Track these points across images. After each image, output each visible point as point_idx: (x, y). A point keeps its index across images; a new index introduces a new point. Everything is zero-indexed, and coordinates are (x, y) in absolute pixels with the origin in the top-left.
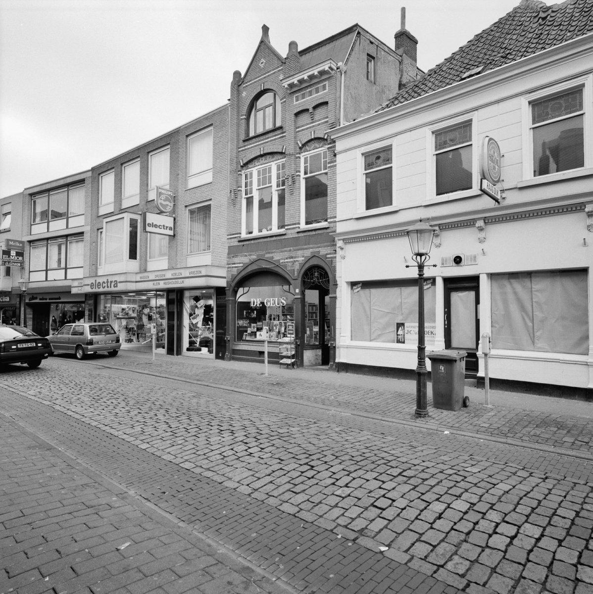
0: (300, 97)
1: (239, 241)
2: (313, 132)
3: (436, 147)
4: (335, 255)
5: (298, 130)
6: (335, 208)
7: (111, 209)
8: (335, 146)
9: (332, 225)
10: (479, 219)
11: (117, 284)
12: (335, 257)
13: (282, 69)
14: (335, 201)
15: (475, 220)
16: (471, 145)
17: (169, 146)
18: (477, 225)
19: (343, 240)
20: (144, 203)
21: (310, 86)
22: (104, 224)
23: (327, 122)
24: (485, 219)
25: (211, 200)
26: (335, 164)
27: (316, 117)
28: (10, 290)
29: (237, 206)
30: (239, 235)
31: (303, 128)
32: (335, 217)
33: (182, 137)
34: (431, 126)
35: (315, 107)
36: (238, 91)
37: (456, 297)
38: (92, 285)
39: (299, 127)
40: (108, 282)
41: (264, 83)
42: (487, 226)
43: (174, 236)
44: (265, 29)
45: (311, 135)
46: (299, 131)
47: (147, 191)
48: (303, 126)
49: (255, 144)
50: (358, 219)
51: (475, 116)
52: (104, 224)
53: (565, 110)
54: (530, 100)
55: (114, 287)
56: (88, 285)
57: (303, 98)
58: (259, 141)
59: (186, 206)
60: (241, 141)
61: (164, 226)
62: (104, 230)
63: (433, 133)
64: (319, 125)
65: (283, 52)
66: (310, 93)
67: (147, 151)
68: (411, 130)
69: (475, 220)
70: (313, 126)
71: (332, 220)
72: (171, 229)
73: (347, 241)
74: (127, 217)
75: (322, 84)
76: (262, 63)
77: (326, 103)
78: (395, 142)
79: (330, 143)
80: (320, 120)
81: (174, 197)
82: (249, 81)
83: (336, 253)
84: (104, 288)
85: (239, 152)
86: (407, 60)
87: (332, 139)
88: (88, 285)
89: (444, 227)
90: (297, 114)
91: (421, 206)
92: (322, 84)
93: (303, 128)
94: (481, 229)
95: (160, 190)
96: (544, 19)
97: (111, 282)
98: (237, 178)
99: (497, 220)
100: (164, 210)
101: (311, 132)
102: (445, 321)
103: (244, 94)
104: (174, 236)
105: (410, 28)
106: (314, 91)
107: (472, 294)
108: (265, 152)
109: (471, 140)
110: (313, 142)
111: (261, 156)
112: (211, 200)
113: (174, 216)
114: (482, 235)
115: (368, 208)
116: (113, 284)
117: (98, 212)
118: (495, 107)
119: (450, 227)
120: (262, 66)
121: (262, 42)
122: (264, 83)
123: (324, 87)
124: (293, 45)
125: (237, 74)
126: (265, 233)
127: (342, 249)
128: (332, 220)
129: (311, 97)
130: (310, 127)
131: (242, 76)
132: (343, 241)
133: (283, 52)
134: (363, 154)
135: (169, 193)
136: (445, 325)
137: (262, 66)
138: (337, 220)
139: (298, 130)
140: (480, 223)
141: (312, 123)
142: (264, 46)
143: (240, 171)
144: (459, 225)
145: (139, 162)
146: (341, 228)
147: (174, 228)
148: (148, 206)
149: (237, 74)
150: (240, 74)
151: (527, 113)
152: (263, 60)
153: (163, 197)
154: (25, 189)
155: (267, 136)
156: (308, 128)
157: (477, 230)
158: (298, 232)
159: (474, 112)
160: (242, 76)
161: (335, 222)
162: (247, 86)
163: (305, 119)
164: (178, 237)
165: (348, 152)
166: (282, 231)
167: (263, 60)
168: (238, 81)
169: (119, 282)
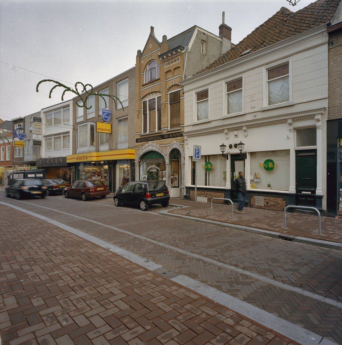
0: (170, 63)
1: (141, 136)
2: (174, 82)
3: (227, 90)
4: (184, 143)
5: (167, 80)
6: (183, 120)
7: (82, 119)
8: (183, 89)
9: (182, 128)
10: (289, 119)
11: (87, 157)
12: (184, 144)
13: (159, 50)
14: (183, 116)
15: (242, 127)
16: (289, 76)
17: (108, 88)
18: (316, 118)
19: (187, 136)
20: (97, 116)
21: (172, 58)
22: (79, 127)
23: (180, 77)
24: (247, 126)
25: (128, 115)
26: (184, 97)
27: (175, 74)
28: (36, 161)
29: (140, 119)
30: (141, 133)
31: (169, 79)
32: (184, 124)
33: (114, 84)
34: (225, 80)
35: (175, 69)
36: (140, 60)
37: (237, 163)
38: (77, 158)
39: (167, 79)
40: (83, 157)
41: (151, 57)
42: (229, 132)
43: (111, 133)
44: (152, 28)
45: (173, 83)
46: (167, 81)
47: (99, 111)
48: (169, 78)
49: (148, 87)
50: (193, 125)
51: (291, 60)
52: (79, 127)
53: (205, 97)
54: (267, 68)
55: (86, 159)
56: (75, 158)
57: (169, 65)
58: (150, 86)
59: (117, 118)
60: (141, 86)
61: (106, 129)
62: (79, 130)
63: (226, 83)
64: (176, 78)
65: (160, 40)
66: (172, 62)
67: (98, 90)
68: (309, 49)
69: (314, 115)
70: (174, 79)
71: (182, 126)
72: (109, 130)
73: (189, 136)
74: (89, 124)
75: (178, 58)
76: (151, 46)
77: (179, 67)
78: (210, 88)
79: (182, 87)
80: (177, 76)
81: (111, 114)
82: (145, 55)
83: (184, 142)
84: (82, 159)
85: (140, 91)
86: (225, 40)
87: (182, 85)
88: (75, 158)
89: (299, 119)
90: (166, 73)
91: (260, 111)
92: (178, 58)
93: (169, 79)
94: (245, 131)
95: (104, 111)
96: (285, 21)
97: (85, 157)
98: (139, 104)
99: (282, 122)
100: (106, 121)
101: (173, 82)
102: (231, 175)
103: (142, 62)
104: (111, 133)
105: (228, 23)
106: (174, 61)
107: (243, 162)
108: (152, 91)
109: (288, 73)
110: (174, 86)
111: (150, 93)
112: (128, 115)
113: (111, 123)
114: (246, 134)
115: (269, 105)
116: (85, 157)
117: (76, 121)
118: (251, 71)
119: (280, 122)
120: (150, 47)
121: (150, 35)
122: (151, 57)
123: (178, 59)
124: (165, 37)
125: (139, 51)
126: (145, 134)
127: (186, 140)
128: (182, 126)
129: (172, 64)
130: (172, 79)
131: (142, 52)
132: (228, 130)
133: (160, 40)
134: (196, 93)
135: (108, 112)
136: (231, 177)
137: (150, 47)
138: (184, 125)
139: (167, 80)
140: (244, 128)
141: (173, 77)
142: (152, 37)
143: (141, 101)
144: (271, 123)
145: (108, 90)
146: (186, 130)
147: (111, 130)
148: (98, 118)
149: (139, 51)
150: (141, 52)
151: (224, 87)
152: (151, 45)
153: (105, 114)
154: (42, 109)
155: (153, 83)
156: (171, 80)
157: (288, 125)
158: (167, 132)
159: (242, 74)
160: (142, 52)
161: (184, 127)
162: (143, 58)
163: (170, 75)
164: (113, 134)
165: (316, 48)
166: (160, 131)
167: (151, 45)
168: (140, 55)
169: (89, 157)
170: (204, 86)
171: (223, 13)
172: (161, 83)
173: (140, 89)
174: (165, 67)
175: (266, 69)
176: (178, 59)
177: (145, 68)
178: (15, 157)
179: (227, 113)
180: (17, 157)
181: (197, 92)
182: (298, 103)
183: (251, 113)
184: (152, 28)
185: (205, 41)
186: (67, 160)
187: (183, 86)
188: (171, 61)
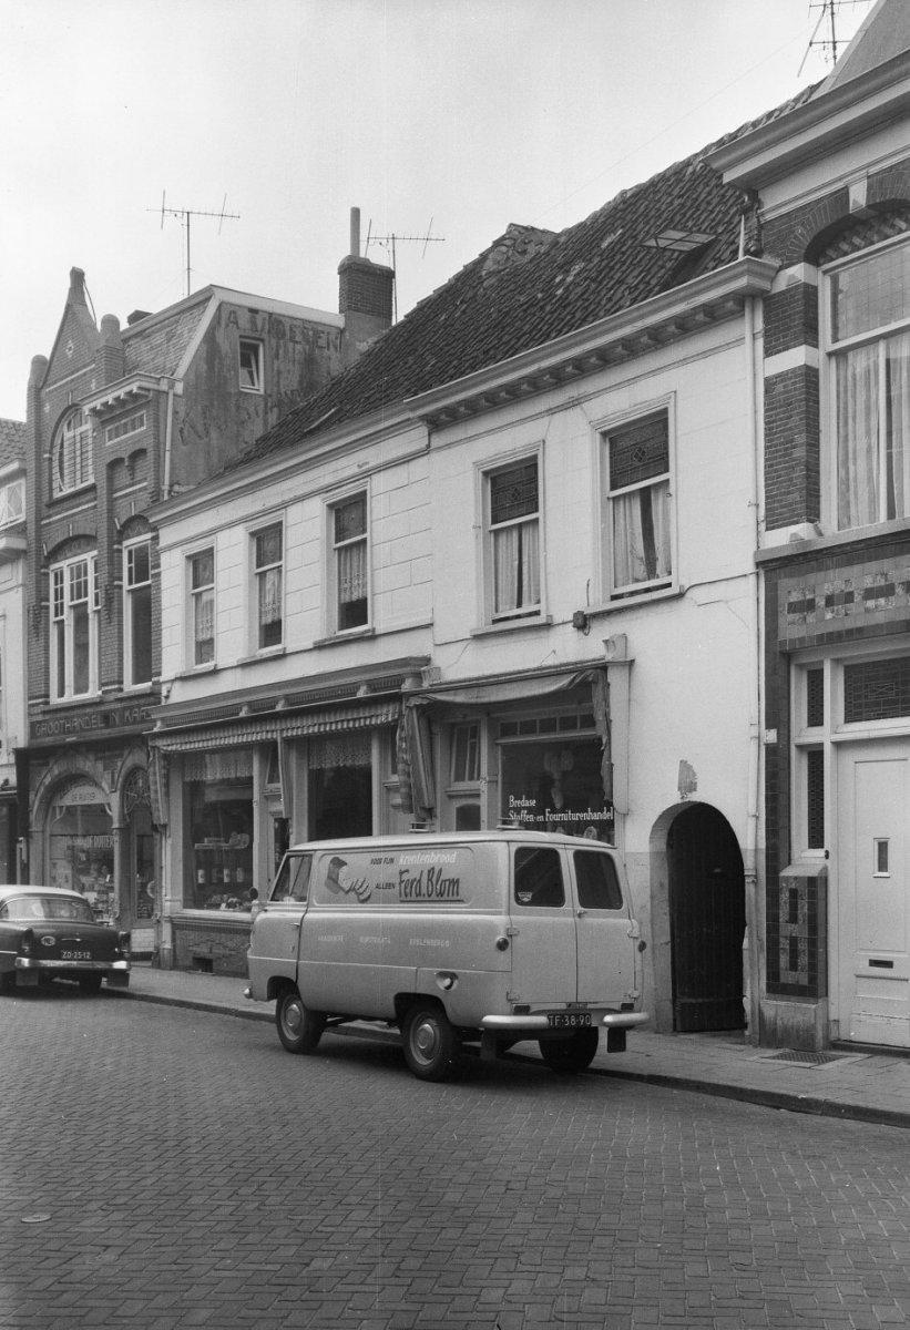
27: (139, 476)
51: (378, 486)
105: (377, 256)
141: (132, 485)
167: (70, 344)
170: (265, 513)
171: (356, 213)
172: (145, 484)
173: (42, 519)
174: (108, 444)
175: (328, 505)
176: (141, 417)
177: (54, 436)
178: (55, 700)
179: (516, 602)
180: (70, 697)
181: (492, 470)
182: (408, 627)
183: (297, 652)
184: (78, 277)
185: (262, 340)
186: (907, 731)
187: (155, 529)
188: (123, 422)
